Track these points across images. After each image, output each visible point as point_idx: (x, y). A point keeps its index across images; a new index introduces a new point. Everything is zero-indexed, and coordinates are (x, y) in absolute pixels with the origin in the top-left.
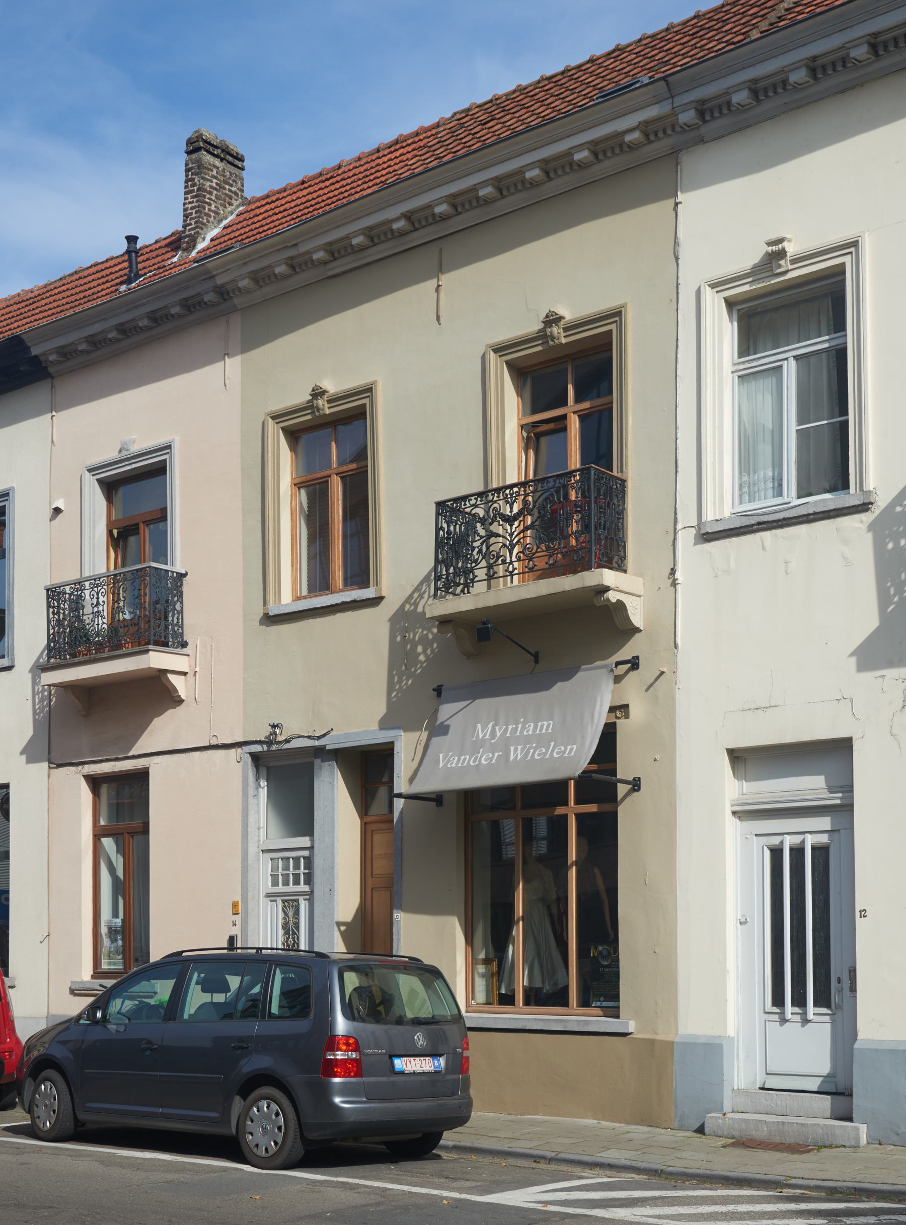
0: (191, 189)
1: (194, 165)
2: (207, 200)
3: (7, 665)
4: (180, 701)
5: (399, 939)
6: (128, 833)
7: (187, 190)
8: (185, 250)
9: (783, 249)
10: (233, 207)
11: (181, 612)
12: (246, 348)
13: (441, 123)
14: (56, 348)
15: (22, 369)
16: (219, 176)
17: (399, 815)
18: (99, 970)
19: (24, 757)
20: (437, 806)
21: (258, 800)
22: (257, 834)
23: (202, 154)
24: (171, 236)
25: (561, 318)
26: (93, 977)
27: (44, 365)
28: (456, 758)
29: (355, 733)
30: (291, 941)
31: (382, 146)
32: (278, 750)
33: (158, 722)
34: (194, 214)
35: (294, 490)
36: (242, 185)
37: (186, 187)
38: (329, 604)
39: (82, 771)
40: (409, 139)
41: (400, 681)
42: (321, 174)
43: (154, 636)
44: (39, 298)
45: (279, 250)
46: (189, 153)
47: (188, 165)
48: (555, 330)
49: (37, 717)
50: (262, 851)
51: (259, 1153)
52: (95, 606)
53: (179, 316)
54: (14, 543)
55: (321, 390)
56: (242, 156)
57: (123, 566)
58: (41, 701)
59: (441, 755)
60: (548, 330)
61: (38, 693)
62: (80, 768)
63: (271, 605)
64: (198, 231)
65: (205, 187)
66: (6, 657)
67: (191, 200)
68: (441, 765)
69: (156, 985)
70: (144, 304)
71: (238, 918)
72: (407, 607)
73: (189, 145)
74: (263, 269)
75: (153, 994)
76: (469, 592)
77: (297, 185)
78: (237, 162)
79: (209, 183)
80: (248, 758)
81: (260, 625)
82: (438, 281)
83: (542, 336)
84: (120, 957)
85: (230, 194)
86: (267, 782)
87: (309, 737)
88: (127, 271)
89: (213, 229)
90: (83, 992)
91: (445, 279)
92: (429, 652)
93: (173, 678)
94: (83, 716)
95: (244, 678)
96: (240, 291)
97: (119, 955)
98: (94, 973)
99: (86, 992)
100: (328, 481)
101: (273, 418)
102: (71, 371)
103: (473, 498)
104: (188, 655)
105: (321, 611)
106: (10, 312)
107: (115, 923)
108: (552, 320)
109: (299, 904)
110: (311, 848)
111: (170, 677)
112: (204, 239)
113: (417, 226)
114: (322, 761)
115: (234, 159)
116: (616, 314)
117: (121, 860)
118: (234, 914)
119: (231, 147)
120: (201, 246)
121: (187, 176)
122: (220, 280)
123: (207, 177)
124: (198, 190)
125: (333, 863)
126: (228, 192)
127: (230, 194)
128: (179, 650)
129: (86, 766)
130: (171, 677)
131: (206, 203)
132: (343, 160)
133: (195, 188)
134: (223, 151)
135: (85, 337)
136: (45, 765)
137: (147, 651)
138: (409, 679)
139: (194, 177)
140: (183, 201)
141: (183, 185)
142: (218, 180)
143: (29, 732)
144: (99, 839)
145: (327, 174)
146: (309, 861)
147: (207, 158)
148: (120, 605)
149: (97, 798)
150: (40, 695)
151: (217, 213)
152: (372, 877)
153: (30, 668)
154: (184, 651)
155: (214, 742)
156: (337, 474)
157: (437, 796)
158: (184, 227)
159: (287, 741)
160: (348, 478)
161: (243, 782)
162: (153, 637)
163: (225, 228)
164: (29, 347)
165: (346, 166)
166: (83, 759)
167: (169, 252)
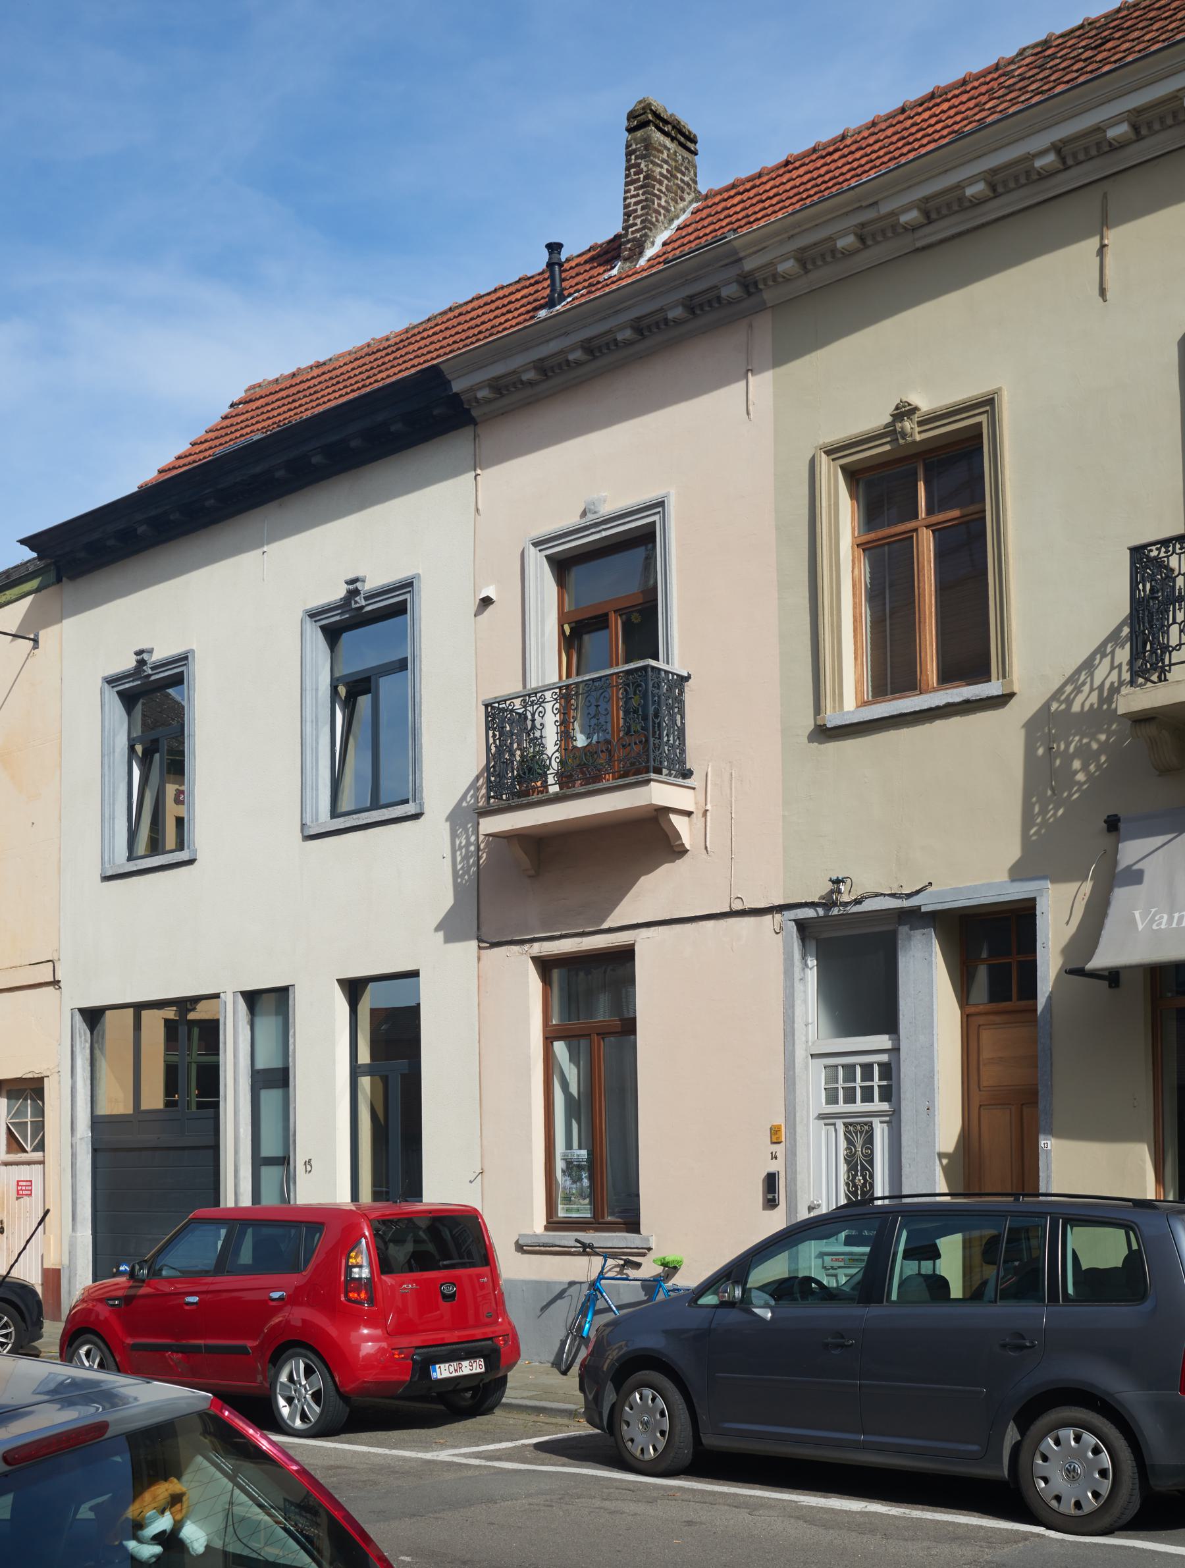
0: (634, 177)
1: (639, 146)
2: (656, 192)
3: (413, 813)
4: (682, 852)
5: (1049, 1177)
6: (597, 1034)
7: (629, 179)
8: (626, 260)
9: (357, 588)
10: (685, 203)
11: (682, 731)
12: (780, 358)
13: (1002, 64)
14: (488, 380)
15: (436, 412)
16: (670, 161)
17: (1047, 1000)
18: (555, 1219)
19: (441, 934)
20: (1110, 986)
21: (805, 985)
22: (804, 1033)
23: (651, 130)
24: (589, 250)
25: (916, 409)
26: (547, 1228)
27: (466, 406)
28: (1166, 916)
29: (968, 888)
30: (859, 1180)
31: (908, 104)
32: (842, 915)
33: (646, 882)
34: (639, 210)
35: (856, 553)
36: (695, 175)
37: (627, 176)
38: (925, 707)
39: (530, 951)
40: (829, 146)
41: (1044, 811)
42: (814, 150)
43: (654, 761)
44: (406, 343)
45: (846, 214)
46: (630, 130)
47: (631, 145)
48: (907, 425)
49: (459, 880)
50: (812, 1055)
51: (633, 1450)
52: (594, 717)
53: (628, 343)
54: (420, 649)
55: (910, 407)
56: (695, 136)
57: (578, 674)
58: (466, 858)
59: (1137, 914)
60: (899, 425)
61: (460, 848)
62: (526, 947)
63: (828, 713)
64: (646, 233)
65: (655, 174)
66: (410, 802)
67: (635, 193)
68: (1140, 927)
69: (650, 1238)
70: (629, 308)
71: (780, 1149)
72: (1054, 706)
73: (632, 120)
74: (815, 244)
75: (646, 1251)
76: (1166, 680)
77: (778, 168)
78: (689, 144)
79: (658, 170)
80: (793, 927)
81: (809, 742)
82: (1102, 239)
83: (891, 432)
84: (587, 1201)
85: (682, 185)
86: (817, 960)
87: (893, 895)
88: (548, 291)
89: (663, 231)
90: (538, 1248)
91: (1112, 236)
92: (1092, 768)
93: (675, 819)
94: (530, 877)
95: (784, 816)
96: (616, 345)
97: (584, 1199)
98: (548, 1222)
99: (542, 1248)
100: (912, 537)
101: (828, 453)
102: (504, 413)
103: (1154, 548)
104: (694, 789)
105: (908, 718)
106: (364, 365)
107: (578, 1155)
108: (904, 412)
109: (872, 1129)
110: (895, 1050)
111: (674, 818)
112: (653, 243)
113: (1070, 162)
114: (911, 929)
115: (685, 139)
116: (988, 403)
117: (575, 1071)
118: (773, 1143)
119: (682, 124)
120: (650, 252)
121: (628, 161)
122: (749, 265)
123: (657, 160)
124: (646, 178)
125: (932, 1071)
126: (679, 183)
127: (682, 185)
128: (680, 781)
129: (536, 945)
130: (674, 818)
131: (655, 195)
132: (848, 129)
133: (642, 176)
134: (674, 127)
135: (534, 362)
136: (474, 944)
137: (647, 782)
138: (1059, 809)
139: (639, 161)
140: (623, 195)
141: (623, 173)
142: (669, 165)
143: (447, 900)
144: (552, 1043)
145: (824, 149)
146: (888, 1071)
147: (657, 136)
148: (536, 735)
149: (548, 987)
150: (464, 850)
151: (668, 210)
152: (980, 1090)
153: (447, 814)
154: (687, 782)
155: (737, 906)
156: (927, 527)
157: (1110, 973)
158: (626, 229)
159: (858, 902)
160: (886, 548)
161: (785, 960)
162: (652, 763)
163: (679, 229)
164: (450, 381)
165: (853, 135)
166: (531, 935)
167: (596, 267)
